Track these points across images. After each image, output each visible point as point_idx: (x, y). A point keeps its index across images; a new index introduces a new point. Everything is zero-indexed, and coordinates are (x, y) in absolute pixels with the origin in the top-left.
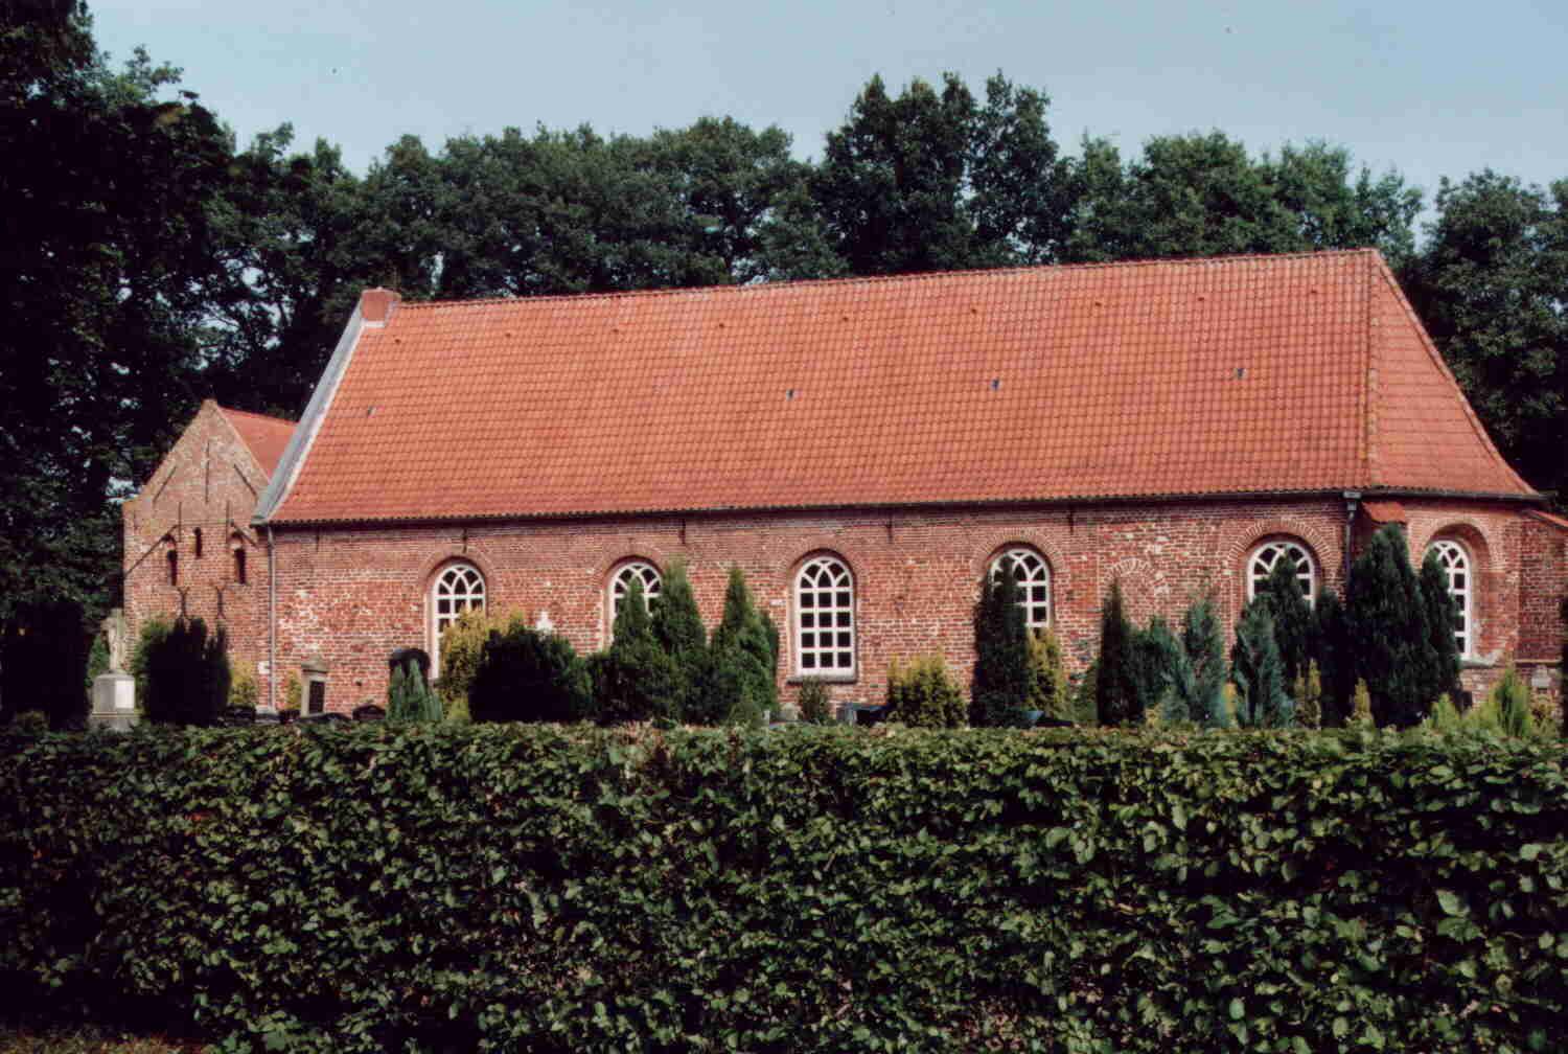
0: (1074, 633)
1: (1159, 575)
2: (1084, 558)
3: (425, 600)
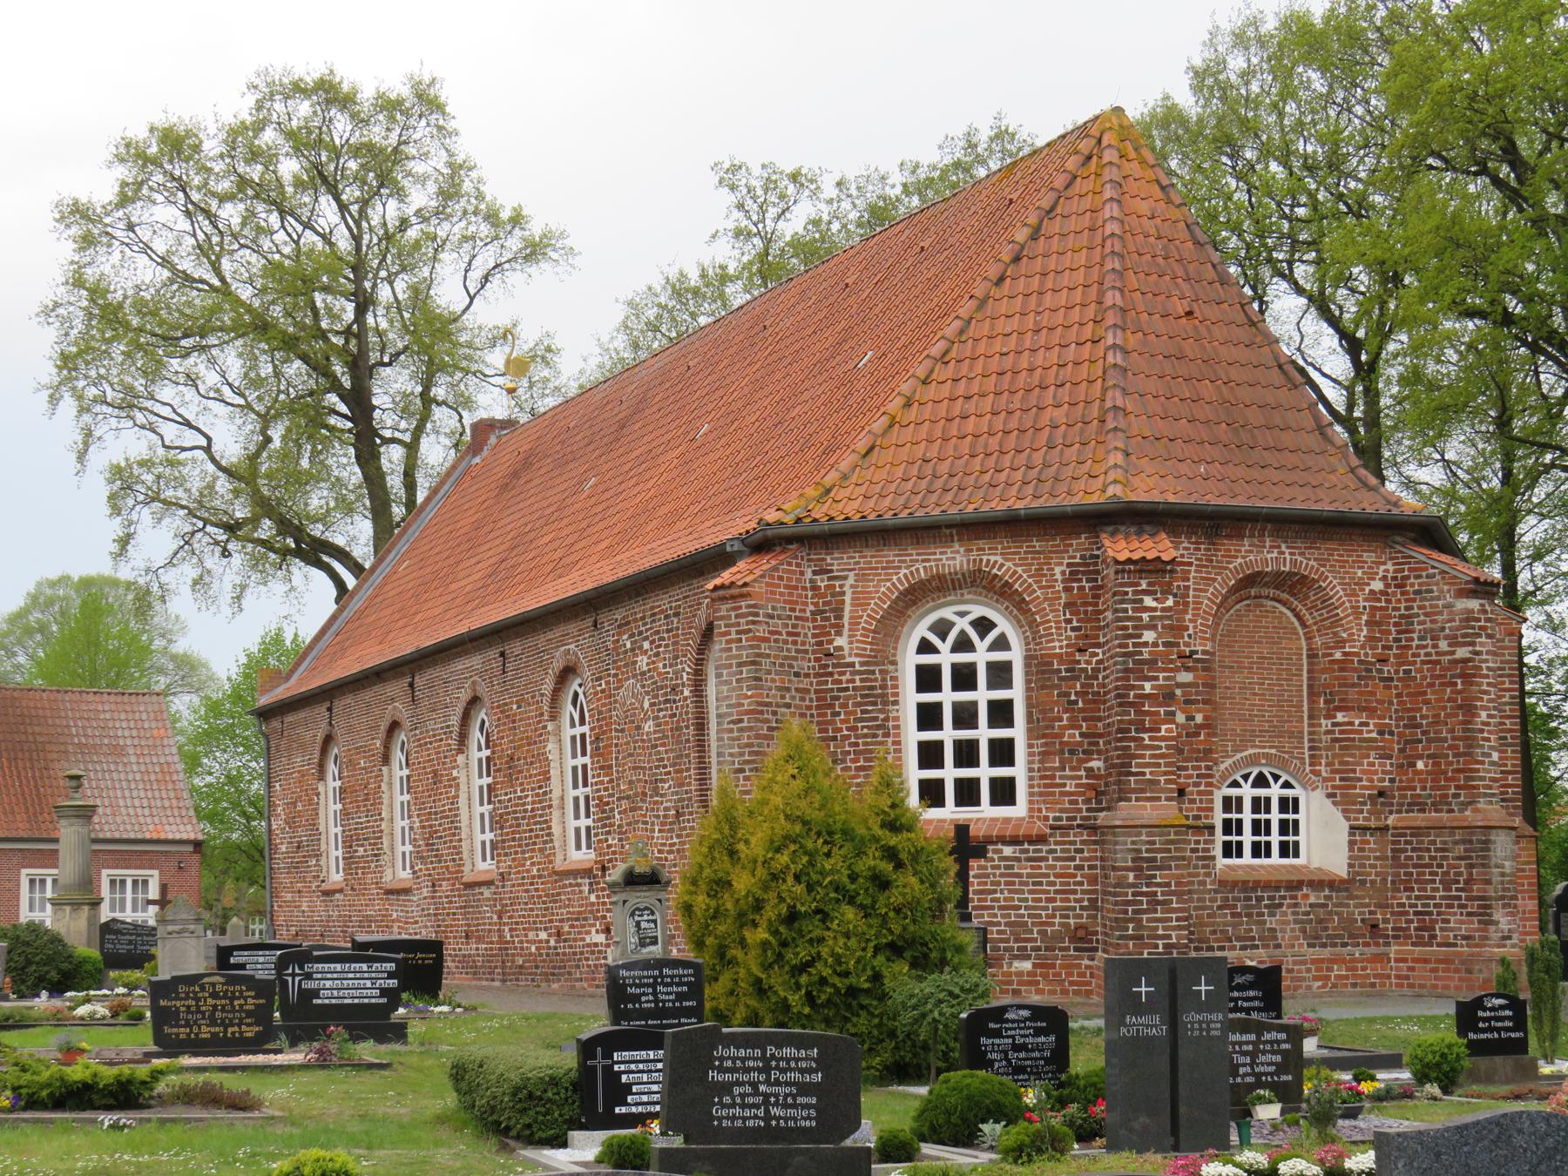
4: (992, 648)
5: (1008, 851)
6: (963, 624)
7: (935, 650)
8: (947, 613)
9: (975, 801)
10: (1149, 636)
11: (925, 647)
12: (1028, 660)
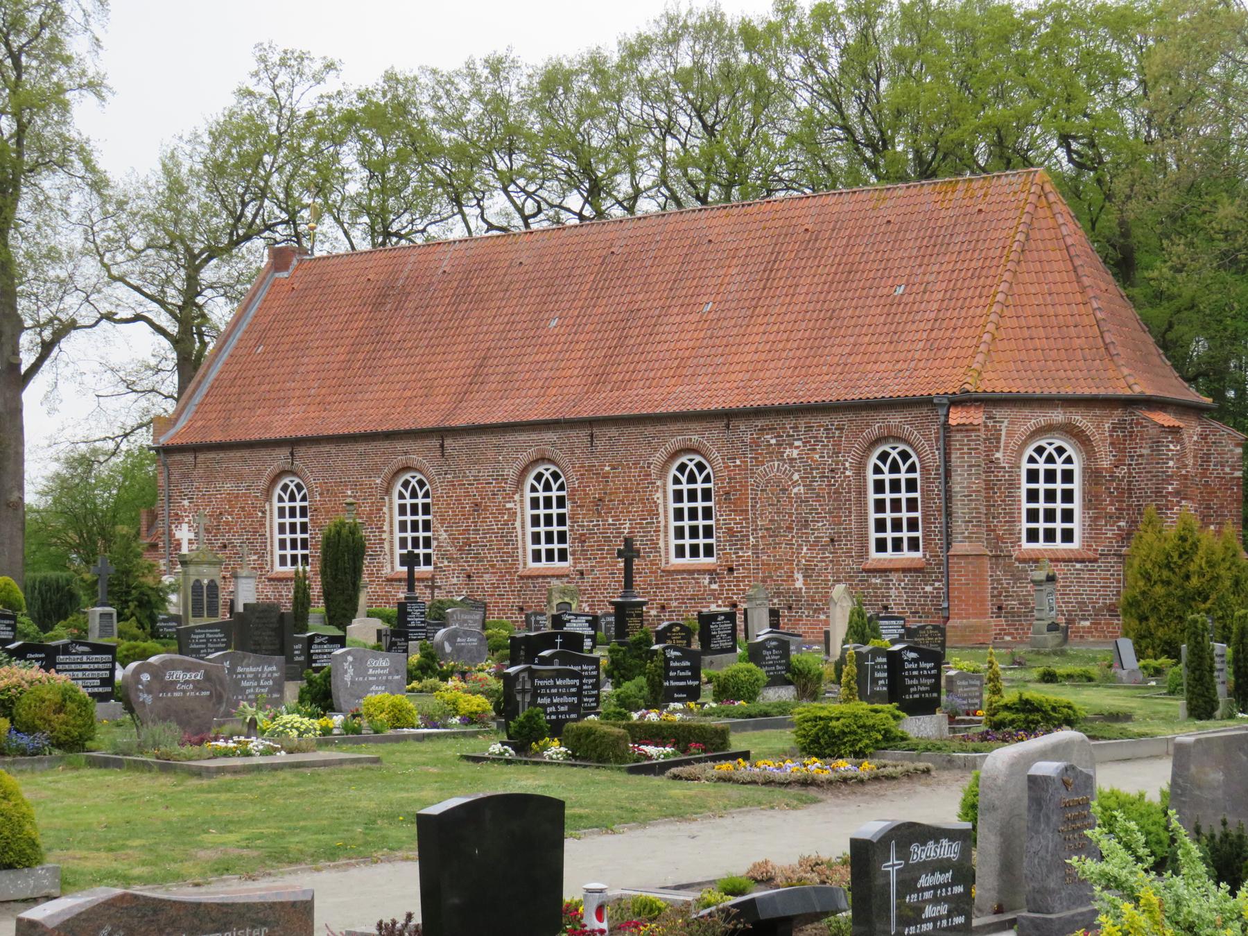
0: (730, 529)
1: (796, 477)
2: (738, 462)
3: (267, 507)
4: (908, 471)
5: (1078, 566)
6: (1050, 449)
7: (882, 472)
8: (1043, 443)
9: (1037, 540)
10: (1171, 463)
11: (1032, 460)
12: (1085, 470)
